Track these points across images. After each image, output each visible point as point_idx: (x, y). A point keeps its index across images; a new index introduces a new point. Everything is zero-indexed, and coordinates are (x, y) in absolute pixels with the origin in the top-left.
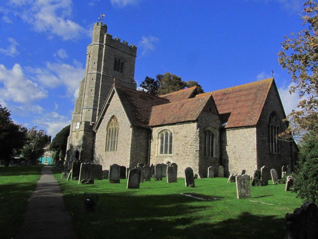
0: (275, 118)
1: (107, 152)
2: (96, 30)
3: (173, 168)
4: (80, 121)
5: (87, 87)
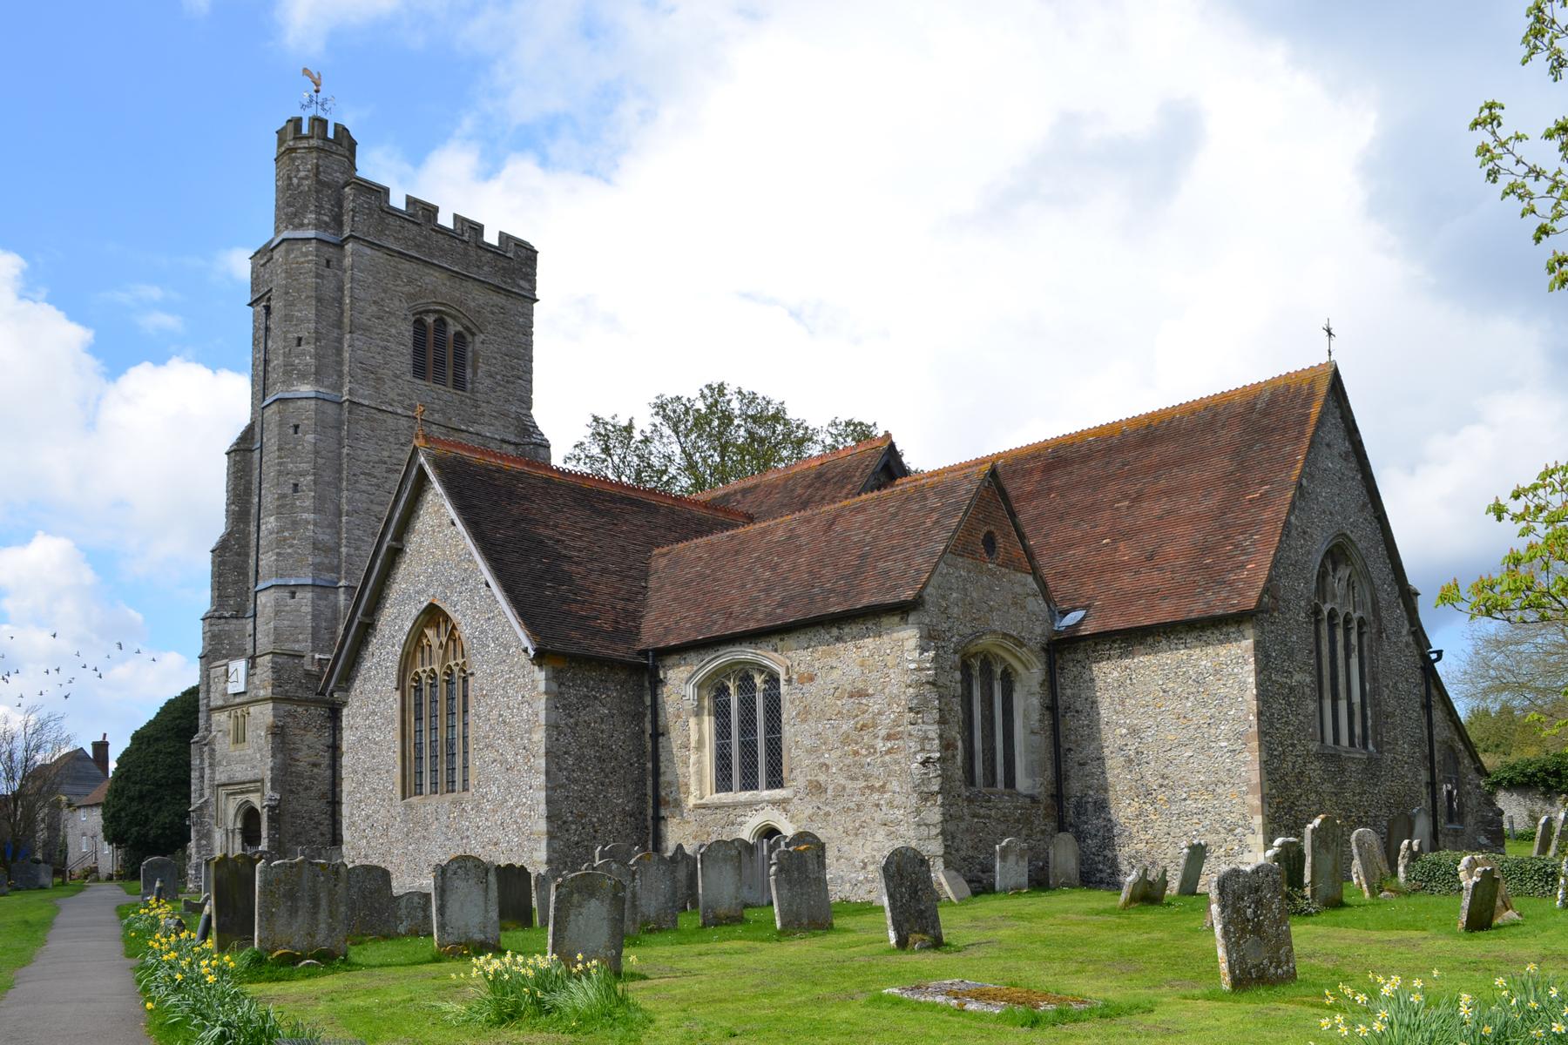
0: (1343, 572)
1: (414, 800)
2: (293, 160)
3: (803, 861)
4: (250, 652)
5: (270, 472)
